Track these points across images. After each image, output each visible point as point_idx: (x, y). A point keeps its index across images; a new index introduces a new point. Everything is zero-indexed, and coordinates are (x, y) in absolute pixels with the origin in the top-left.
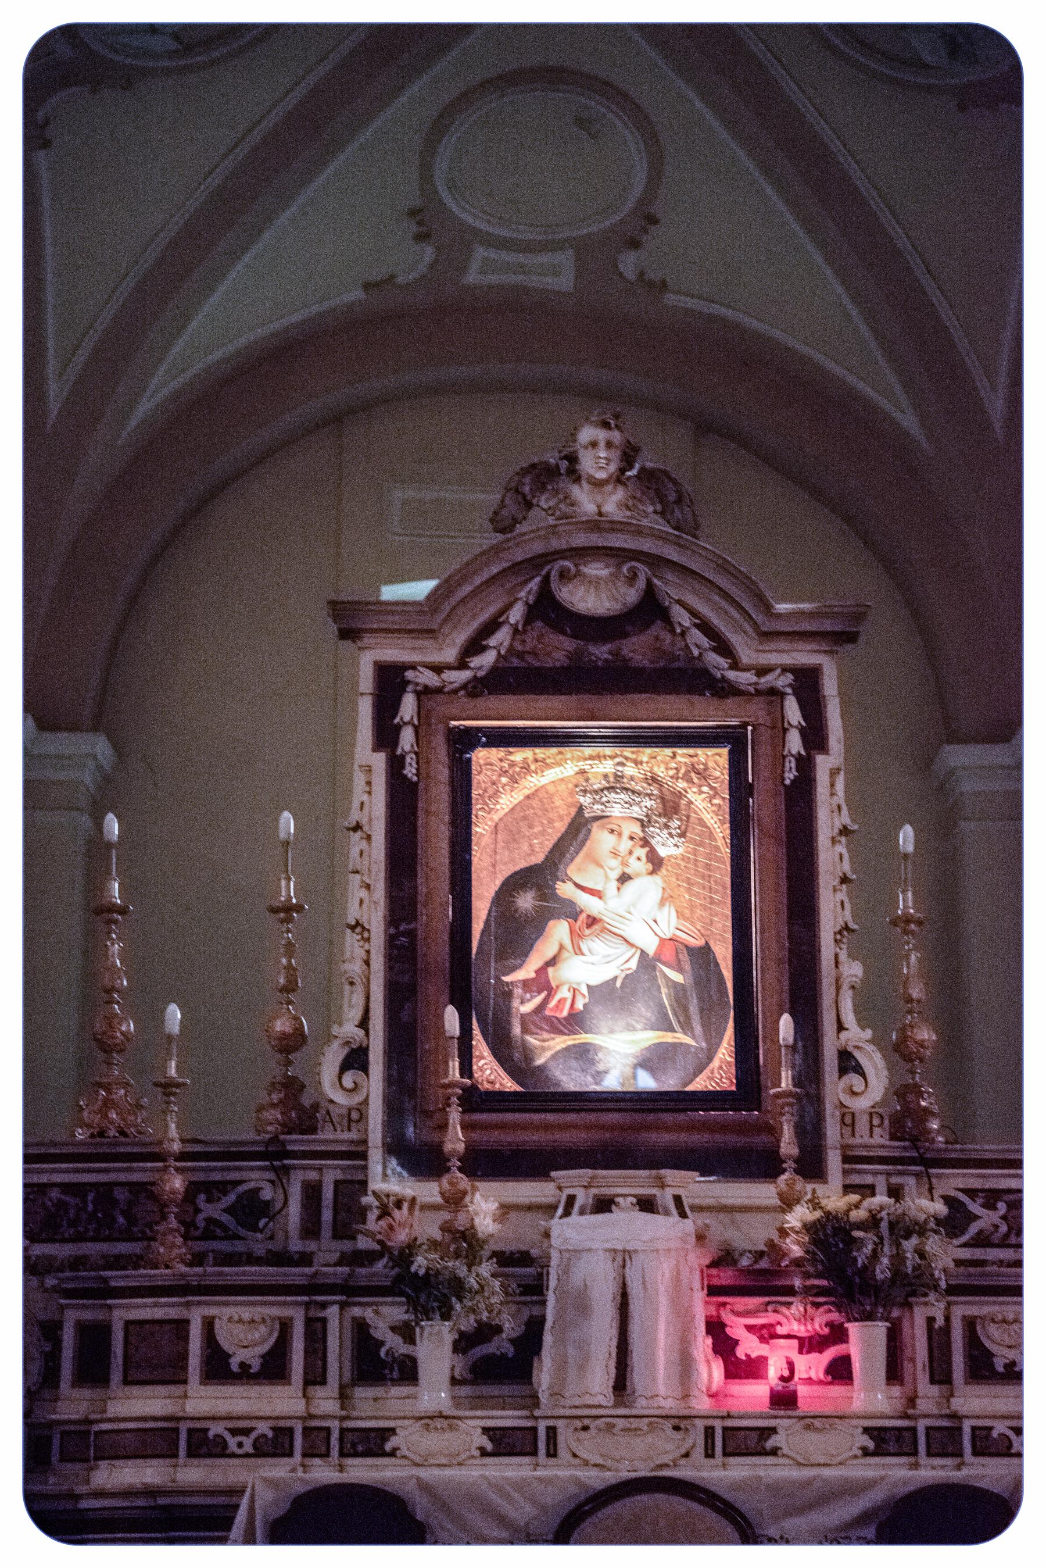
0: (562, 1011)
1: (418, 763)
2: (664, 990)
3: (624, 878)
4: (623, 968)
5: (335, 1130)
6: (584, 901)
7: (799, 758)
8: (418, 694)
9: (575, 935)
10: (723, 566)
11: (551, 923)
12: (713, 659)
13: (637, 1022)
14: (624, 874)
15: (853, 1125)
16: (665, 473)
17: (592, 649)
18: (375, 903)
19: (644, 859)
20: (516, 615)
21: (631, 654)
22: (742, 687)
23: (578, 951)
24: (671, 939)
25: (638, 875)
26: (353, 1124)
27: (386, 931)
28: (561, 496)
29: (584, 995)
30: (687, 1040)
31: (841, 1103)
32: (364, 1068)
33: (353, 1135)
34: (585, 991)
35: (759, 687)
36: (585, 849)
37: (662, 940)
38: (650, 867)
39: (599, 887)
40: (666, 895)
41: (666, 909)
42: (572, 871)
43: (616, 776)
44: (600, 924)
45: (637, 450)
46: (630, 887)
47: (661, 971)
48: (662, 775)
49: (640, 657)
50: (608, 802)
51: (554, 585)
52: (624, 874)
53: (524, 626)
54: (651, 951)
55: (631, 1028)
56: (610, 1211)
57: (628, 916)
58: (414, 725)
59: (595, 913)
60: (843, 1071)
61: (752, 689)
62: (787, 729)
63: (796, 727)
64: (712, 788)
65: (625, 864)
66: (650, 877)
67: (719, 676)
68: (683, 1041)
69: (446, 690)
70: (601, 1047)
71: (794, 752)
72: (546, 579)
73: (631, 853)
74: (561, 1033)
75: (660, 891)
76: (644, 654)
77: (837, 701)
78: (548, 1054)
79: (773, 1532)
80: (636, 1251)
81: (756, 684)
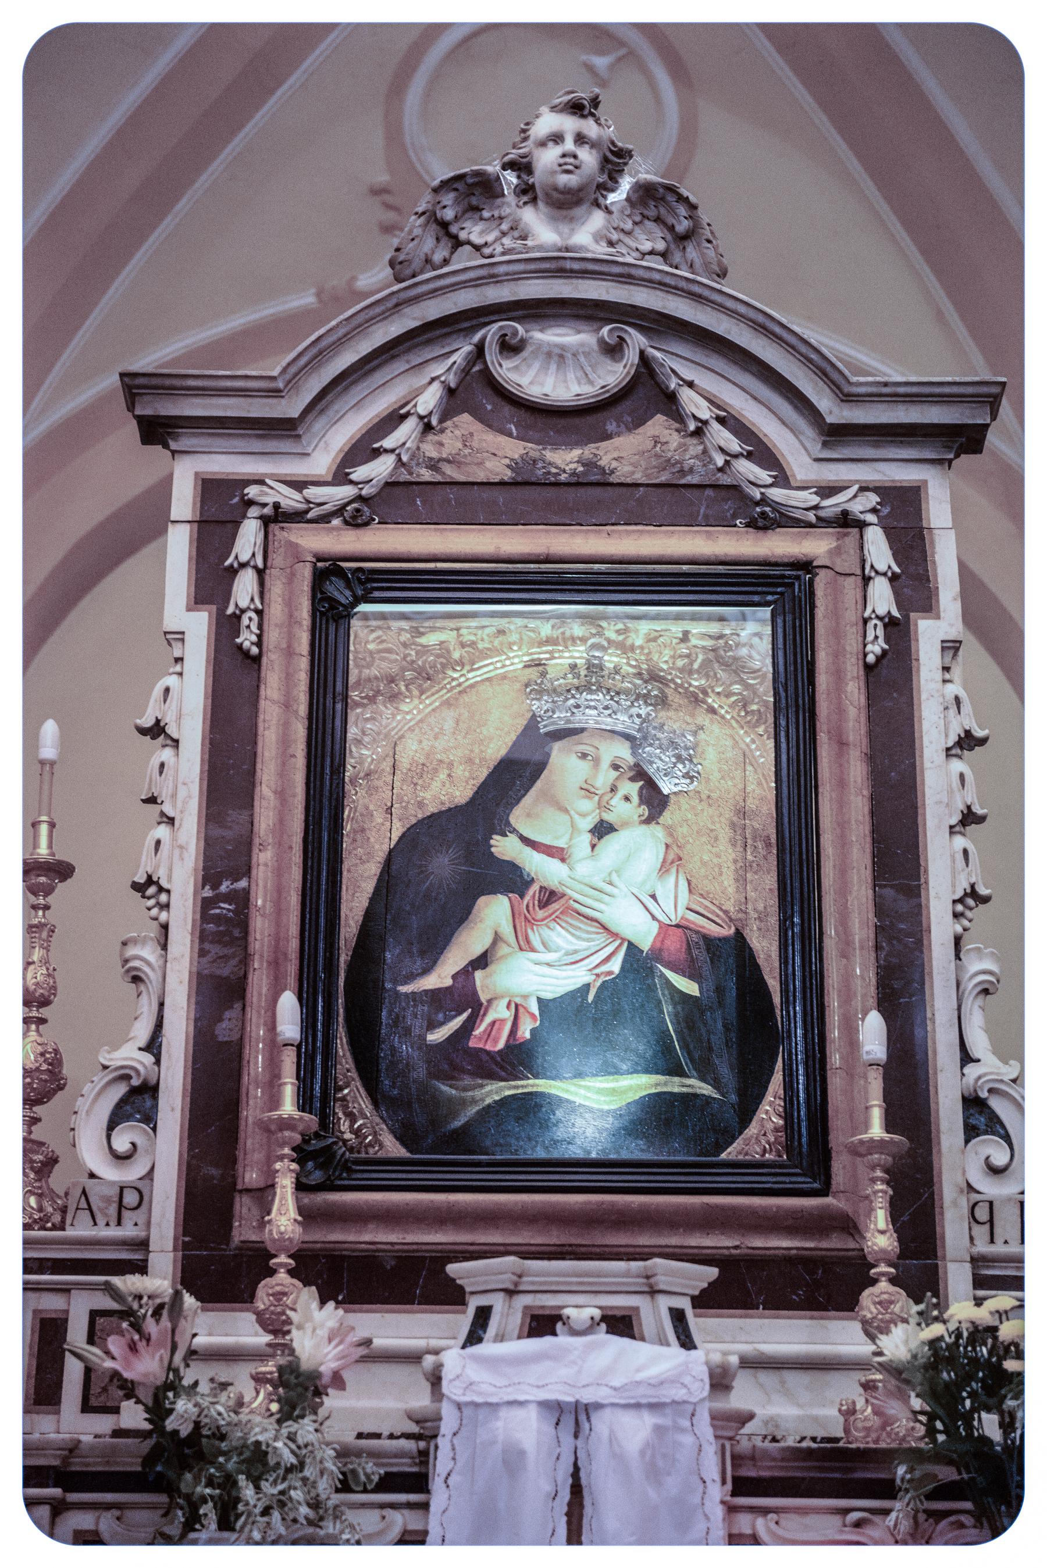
0: (496, 1041)
1: (260, 626)
2: (667, 1009)
3: (602, 830)
4: (597, 971)
5: (95, 1224)
6: (534, 863)
7: (890, 623)
8: (266, 521)
9: (521, 921)
10: (764, 327)
11: (482, 900)
12: (748, 469)
13: (623, 1060)
14: (602, 821)
15: (991, 1221)
16: (671, 189)
17: (550, 455)
18: (181, 847)
19: (635, 799)
20: (429, 401)
21: (614, 464)
22: (798, 514)
23: (526, 946)
24: (677, 926)
25: (626, 824)
26: (126, 1214)
27: (195, 893)
28: (505, 227)
29: (533, 1016)
30: (705, 1089)
31: (969, 1185)
32: (150, 1119)
33: (128, 1231)
34: (534, 1008)
35: (822, 513)
36: (539, 784)
37: (664, 928)
38: (644, 810)
39: (561, 843)
40: (671, 856)
41: (671, 879)
42: (517, 817)
43: (590, 666)
44: (562, 901)
45: (623, 154)
46: (612, 844)
47: (662, 975)
48: (665, 667)
49: (630, 468)
50: (578, 706)
51: (492, 355)
52: (602, 821)
53: (441, 421)
54: (645, 944)
55: (610, 1070)
56: (554, 1334)
57: (608, 888)
58: (255, 567)
59: (553, 883)
60: (971, 1132)
61: (811, 517)
62: (870, 578)
63: (885, 574)
64: (747, 686)
65: (603, 806)
66: (644, 827)
67: (758, 496)
68: (699, 1091)
69: (310, 515)
70: (560, 1101)
71: (881, 611)
72: (480, 350)
73: (613, 789)
74: (492, 1076)
75: (662, 849)
76: (635, 465)
77: (952, 535)
78: (473, 1110)
79: (871, 679)
80: (599, 1406)
81: (816, 507)
